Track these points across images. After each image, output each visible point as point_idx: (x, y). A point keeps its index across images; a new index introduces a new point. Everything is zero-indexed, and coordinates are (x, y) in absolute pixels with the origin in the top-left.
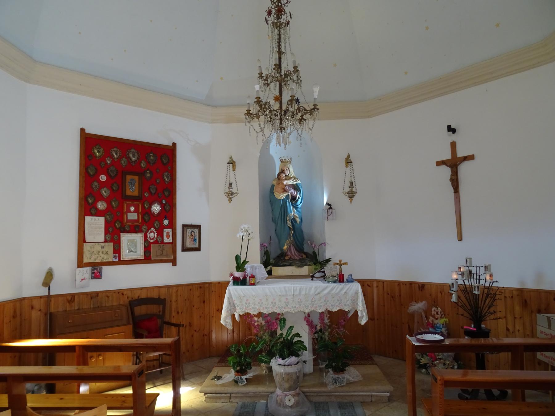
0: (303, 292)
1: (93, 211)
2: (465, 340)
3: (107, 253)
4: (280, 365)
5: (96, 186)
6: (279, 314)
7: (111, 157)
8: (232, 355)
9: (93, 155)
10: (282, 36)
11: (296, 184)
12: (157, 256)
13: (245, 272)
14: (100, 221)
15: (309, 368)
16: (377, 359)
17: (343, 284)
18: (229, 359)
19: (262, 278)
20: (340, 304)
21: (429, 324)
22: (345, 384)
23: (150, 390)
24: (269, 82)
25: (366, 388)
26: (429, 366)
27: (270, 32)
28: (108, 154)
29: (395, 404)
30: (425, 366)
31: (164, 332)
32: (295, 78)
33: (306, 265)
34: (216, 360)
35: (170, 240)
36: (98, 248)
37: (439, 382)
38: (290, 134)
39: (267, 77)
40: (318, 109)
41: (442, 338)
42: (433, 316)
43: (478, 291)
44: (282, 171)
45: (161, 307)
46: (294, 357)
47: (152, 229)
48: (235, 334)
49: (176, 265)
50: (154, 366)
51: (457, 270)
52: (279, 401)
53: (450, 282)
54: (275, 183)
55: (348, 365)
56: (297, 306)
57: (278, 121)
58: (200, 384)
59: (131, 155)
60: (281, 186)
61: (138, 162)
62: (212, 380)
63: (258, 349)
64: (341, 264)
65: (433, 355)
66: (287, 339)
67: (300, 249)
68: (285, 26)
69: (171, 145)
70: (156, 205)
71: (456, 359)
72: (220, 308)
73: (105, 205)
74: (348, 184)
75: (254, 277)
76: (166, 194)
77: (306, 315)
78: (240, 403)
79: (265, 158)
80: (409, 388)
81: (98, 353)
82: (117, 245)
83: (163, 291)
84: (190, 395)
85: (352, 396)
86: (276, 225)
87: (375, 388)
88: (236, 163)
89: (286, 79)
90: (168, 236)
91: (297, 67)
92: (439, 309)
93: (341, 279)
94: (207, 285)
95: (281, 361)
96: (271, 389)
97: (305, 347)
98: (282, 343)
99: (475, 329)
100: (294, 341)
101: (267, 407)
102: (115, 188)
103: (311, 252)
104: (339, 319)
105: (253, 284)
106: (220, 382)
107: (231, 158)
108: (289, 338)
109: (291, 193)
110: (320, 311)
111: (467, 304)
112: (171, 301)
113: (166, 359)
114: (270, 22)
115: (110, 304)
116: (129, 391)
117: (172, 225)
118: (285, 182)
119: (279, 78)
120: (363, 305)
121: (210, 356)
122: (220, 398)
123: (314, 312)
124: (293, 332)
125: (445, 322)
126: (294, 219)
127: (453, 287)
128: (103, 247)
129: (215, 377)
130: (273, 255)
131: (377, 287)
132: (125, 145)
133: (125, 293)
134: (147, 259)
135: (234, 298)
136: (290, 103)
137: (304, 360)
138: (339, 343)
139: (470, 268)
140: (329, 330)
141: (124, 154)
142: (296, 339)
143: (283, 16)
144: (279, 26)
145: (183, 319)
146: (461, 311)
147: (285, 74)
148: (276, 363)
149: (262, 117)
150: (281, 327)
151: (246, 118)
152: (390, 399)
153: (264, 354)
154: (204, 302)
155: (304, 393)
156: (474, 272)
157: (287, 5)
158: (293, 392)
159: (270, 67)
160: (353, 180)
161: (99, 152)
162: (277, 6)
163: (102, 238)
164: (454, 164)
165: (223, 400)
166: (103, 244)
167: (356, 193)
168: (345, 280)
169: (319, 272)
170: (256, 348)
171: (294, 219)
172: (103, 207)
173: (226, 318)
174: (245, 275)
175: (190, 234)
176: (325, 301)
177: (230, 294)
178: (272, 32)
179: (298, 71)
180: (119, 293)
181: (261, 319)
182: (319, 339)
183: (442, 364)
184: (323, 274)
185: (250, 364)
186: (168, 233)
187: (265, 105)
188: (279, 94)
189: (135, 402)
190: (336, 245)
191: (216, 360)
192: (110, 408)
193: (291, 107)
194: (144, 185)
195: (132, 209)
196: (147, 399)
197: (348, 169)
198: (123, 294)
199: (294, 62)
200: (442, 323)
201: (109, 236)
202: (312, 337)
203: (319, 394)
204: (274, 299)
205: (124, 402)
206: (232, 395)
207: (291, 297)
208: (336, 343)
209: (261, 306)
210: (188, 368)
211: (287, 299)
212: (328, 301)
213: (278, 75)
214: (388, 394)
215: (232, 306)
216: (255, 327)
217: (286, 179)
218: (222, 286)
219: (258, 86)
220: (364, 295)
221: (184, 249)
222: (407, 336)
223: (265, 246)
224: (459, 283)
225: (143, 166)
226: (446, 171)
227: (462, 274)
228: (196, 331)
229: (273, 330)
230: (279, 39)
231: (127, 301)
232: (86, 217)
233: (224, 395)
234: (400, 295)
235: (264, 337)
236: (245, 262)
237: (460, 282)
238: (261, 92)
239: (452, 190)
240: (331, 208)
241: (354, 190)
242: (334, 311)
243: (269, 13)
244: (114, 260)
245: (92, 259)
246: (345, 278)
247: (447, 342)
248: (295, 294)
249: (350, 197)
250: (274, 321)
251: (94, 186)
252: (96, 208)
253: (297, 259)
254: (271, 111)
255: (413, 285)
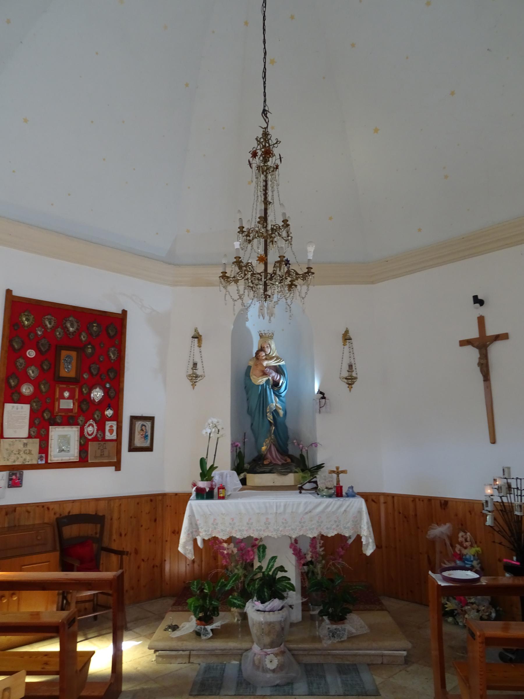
0: (289, 510)
1: (15, 397)
2: (507, 579)
3: (30, 453)
4: (258, 610)
5: (21, 364)
6: (256, 539)
7: (43, 327)
8: (192, 595)
9: (20, 324)
10: (269, 183)
11: (279, 366)
12: (96, 457)
13: (212, 481)
14: (25, 410)
15: (297, 615)
16: (387, 602)
17: (341, 499)
18: (189, 601)
19: (235, 490)
20: (338, 526)
21: (455, 555)
22: (345, 638)
23: (82, 646)
24: (251, 238)
25: (374, 645)
26: (458, 613)
27: (254, 177)
28: (39, 323)
29: (413, 668)
30: (452, 613)
31: (101, 562)
32: (284, 234)
33: (291, 472)
34: (170, 601)
35: (114, 436)
36: (19, 445)
37: (479, 640)
38: (276, 303)
39: (249, 232)
40: (313, 273)
41: (476, 576)
42: (461, 544)
43: (521, 511)
44: (262, 349)
45: (99, 526)
46: (277, 600)
47: (91, 422)
48: (196, 565)
49: (120, 470)
50: (86, 609)
51: (492, 482)
52: (257, 662)
53: (483, 499)
54: (251, 363)
55: (350, 612)
56: (281, 529)
57: (261, 287)
58: (149, 636)
59: (69, 325)
60: (260, 368)
61: (78, 333)
62: (166, 630)
63: (228, 588)
64: (338, 472)
65: (462, 598)
66: (268, 574)
67: (283, 451)
68: (273, 171)
69: (120, 312)
70: (98, 389)
71: (493, 604)
72: (177, 529)
73: (32, 389)
74: (346, 367)
75: (223, 488)
76: (112, 375)
77: (293, 542)
78: (203, 665)
79: (239, 333)
80: (434, 645)
81: (12, 592)
82: (44, 442)
83: (102, 504)
84: (136, 653)
85: (355, 655)
86: (253, 418)
87: (387, 644)
88: (203, 337)
89: (273, 235)
90: (111, 431)
91: (287, 221)
92: (468, 534)
93: (339, 493)
94: (160, 498)
95: (260, 606)
96: (245, 645)
97: (292, 585)
98: (261, 579)
99: (518, 563)
100: (277, 577)
101: (240, 670)
102: (45, 367)
103: (297, 455)
104: (335, 547)
105: (223, 498)
106: (177, 634)
107: (196, 330)
108: (271, 573)
109: (273, 377)
110: (311, 536)
111: (507, 529)
112: (111, 519)
113: (102, 599)
114: (254, 166)
115: (30, 522)
116: (53, 647)
117: (117, 417)
118: (265, 363)
119: (265, 234)
120: (368, 528)
121: (162, 596)
122: (176, 657)
123: (303, 536)
124: (277, 565)
125: (477, 552)
126: (276, 411)
127: (487, 506)
128: (25, 445)
129: (170, 627)
130: (248, 459)
131: (385, 503)
132: (61, 312)
133: (51, 507)
134: (83, 461)
135: (197, 517)
136: (278, 265)
137: (290, 604)
138: (335, 580)
139: (509, 481)
140: (324, 562)
141: (60, 324)
142: (280, 575)
143: (270, 159)
144: (266, 171)
145: (127, 545)
146: (498, 538)
147: (272, 229)
148: (254, 609)
149: (242, 282)
150: (259, 557)
151: (221, 282)
152: (407, 661)
153: (236, 594)
154: (155, 520)
155: (290, 650)
156: (514, 486)
157: (276, 145)
158: (276, 650)
159: (254, 219)
160: (353, 362)
161: (27, 320)
162: (264, 146)
163: (24, 433)
164: (482, 343)
165: (179, 660)
166: (25, 441)
167: (356, 378)
168: (344, 494)
169: (310, 482)
170: (226, 585)
171: (276, 411)
172: (28, 391)
173: (185, 544)
174: (212, 485)
175: (140, 429)
176: (318, 522)
177: (192, 511)
178: (257, 178)
179: (288, 225)
180: (43, 507)
181: (232, 545)
182: (310, 575)
183: (475, 611)
184: (315, 485)
185: (217, 608)
186: (111, 426)
187: (246, 266)
188: (263, 252)
189: (62, 663)
190: (331, 444)
191: (170, 601)
192: (30, 673)
193: (280, 270)
194: (84, 364)
195: (66, 394)
196: (79, 659)
197: (346, 347)
198: (48, 509)
199: (284, 214)
200: (473, 553)
201: (34, 429)
202: (300, 571)
203: (311, 653)
204: (250, 519)
205: (46, 663)
206: (193, 653)
207: (269, 515)
208: (332, 581)
209: (233, 528)
210: (131, 612)
211: (267, 519)
212: (322, 522)
213: (263, 230)
214: (405, 653)
215: (194, 528)
216: (224, 557)
217: (266, 359)
218: (181, 499)
219: (239, 243)
220: (369, 514)
221: (132, 449)
222: (430, 572)
224: (495, 500)
225: (83, 339)
226: (472, 354)
227: (499, 489)
228: (143, 560)
229: (248, 561)
230: (266, 186)
231: (53, 517)
232: (5, 404)
233: (181, 652)
234: (416, 515)
235: (236, 571)
236: (212, 468)
237: (497, 499)
238: (240, 249)
239: (480, 377)
240: (323, 398)
241: (354, 374)
242: (329, 535)
243: (254, 155)
244: (40, 462)
245: (10, 460)
246: (345, 491)
247: (484, 581)
248: (279, 512)
249: (349, 384)
250: (250, 549)
251: (18, 364)
252: (20, 393)
253: (280, 463)
254: (252, 275)
255: (433, 501)
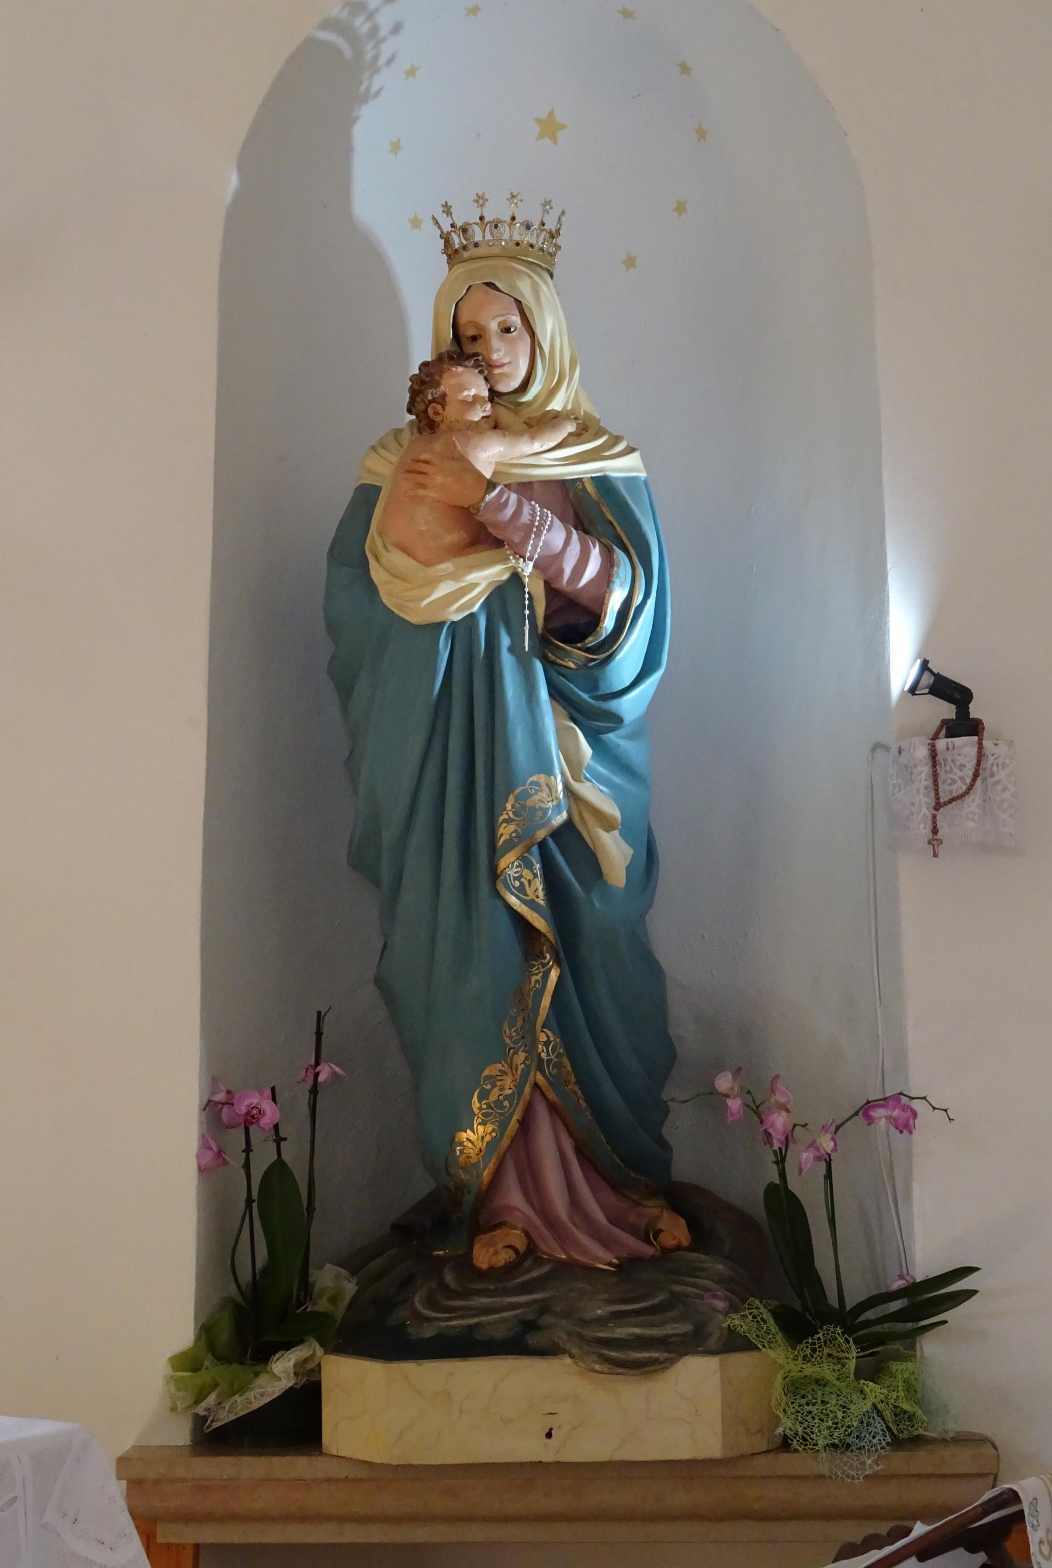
11: (603, 482)
33: (695, 1342)
44: (463, 346)
54: (382, 469)
67: (627, 1158)
86: (389, 912)
103: (743, 1183)
109: (548, 566)
118: (489, 455)
217: (495, 425)
223: (251, 1118)
240: (964, 725)
253: (602, 1258)
